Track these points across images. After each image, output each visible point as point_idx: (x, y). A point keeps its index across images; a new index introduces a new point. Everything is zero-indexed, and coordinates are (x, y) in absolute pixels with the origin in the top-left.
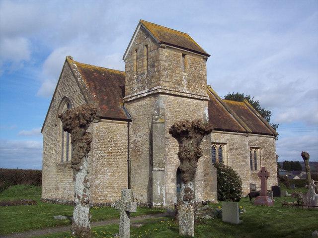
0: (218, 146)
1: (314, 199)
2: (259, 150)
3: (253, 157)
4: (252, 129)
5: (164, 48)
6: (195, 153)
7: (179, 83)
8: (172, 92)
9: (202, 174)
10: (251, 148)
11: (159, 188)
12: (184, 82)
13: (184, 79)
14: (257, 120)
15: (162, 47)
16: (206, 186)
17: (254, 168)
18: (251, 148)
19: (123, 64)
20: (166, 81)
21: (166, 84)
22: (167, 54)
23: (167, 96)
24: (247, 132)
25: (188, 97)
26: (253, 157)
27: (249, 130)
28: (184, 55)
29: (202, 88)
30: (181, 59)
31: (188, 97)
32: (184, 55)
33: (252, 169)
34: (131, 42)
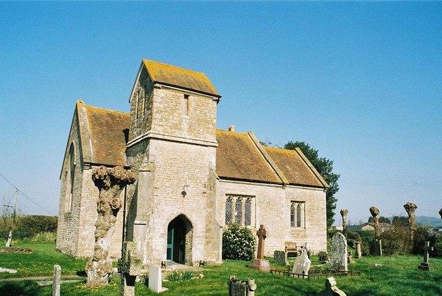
0: (237, 198)
1: (304, 265)
2: (303, 204)
3: (296, 212)
4: (289, 177)
5: (159, 88)
6: (111, 205)
7: (177, 127)
8: (166, 138)
9: (204, 230)
10: (291, 201)
11: (139, 243)
12: (185, 126)
13: (184, 123)
14: (307, 171)
15: (156, 87)
16: (208, 243)
17: (296, 224)
18: (291, 201)
19: (129, 106)
20: (160, 125)
21: (160, 129)
22: (162, 95)
23: (160, 141)
24: (283, 184)
25: (189, 143)
26: (296, 212)
27: (286, 181)
28: (186, 97)
29: (209, 133)
30: (183, 100)
31: (189, 143)
32: (186, 97)
33: (292, 225)
34: (134, 85)
